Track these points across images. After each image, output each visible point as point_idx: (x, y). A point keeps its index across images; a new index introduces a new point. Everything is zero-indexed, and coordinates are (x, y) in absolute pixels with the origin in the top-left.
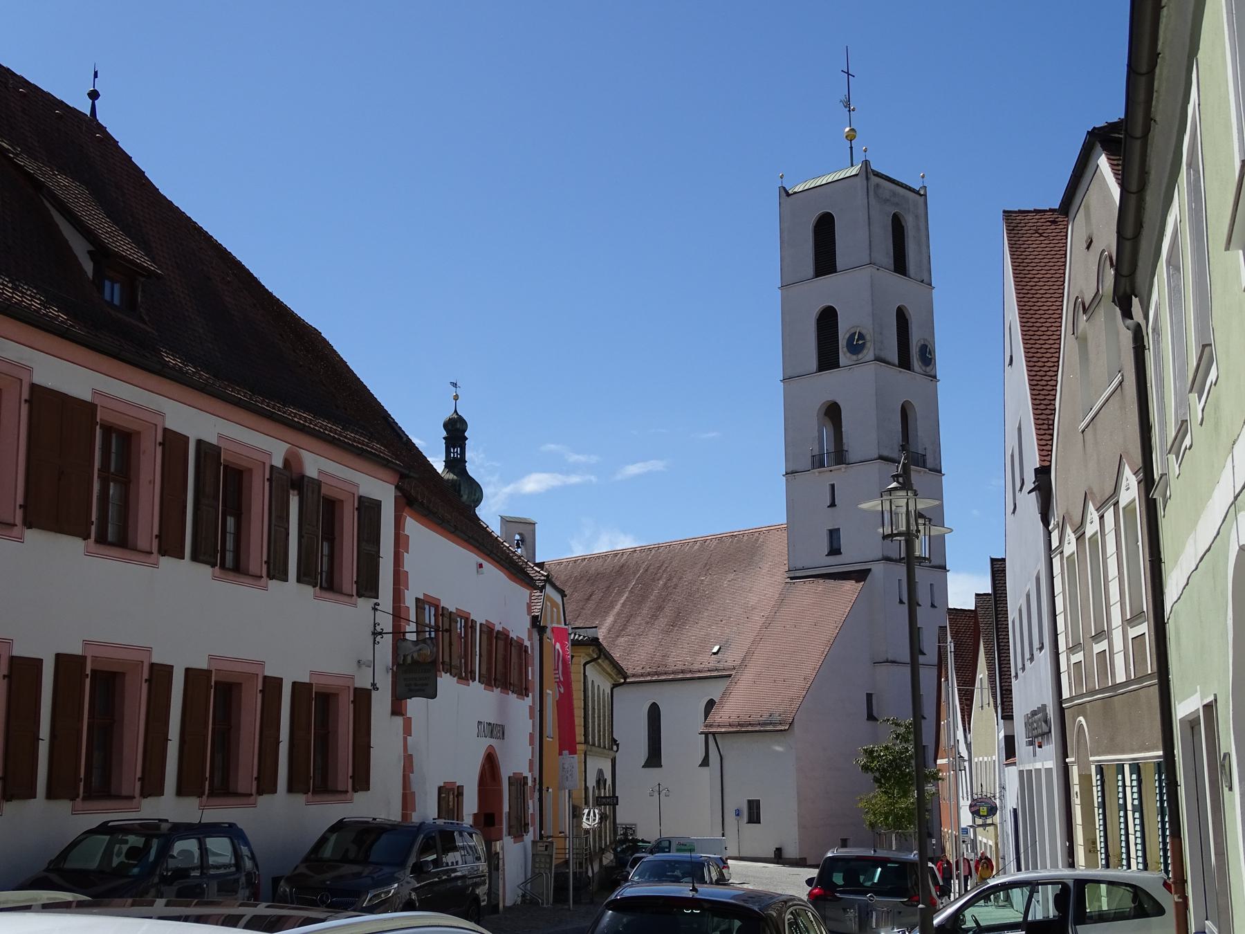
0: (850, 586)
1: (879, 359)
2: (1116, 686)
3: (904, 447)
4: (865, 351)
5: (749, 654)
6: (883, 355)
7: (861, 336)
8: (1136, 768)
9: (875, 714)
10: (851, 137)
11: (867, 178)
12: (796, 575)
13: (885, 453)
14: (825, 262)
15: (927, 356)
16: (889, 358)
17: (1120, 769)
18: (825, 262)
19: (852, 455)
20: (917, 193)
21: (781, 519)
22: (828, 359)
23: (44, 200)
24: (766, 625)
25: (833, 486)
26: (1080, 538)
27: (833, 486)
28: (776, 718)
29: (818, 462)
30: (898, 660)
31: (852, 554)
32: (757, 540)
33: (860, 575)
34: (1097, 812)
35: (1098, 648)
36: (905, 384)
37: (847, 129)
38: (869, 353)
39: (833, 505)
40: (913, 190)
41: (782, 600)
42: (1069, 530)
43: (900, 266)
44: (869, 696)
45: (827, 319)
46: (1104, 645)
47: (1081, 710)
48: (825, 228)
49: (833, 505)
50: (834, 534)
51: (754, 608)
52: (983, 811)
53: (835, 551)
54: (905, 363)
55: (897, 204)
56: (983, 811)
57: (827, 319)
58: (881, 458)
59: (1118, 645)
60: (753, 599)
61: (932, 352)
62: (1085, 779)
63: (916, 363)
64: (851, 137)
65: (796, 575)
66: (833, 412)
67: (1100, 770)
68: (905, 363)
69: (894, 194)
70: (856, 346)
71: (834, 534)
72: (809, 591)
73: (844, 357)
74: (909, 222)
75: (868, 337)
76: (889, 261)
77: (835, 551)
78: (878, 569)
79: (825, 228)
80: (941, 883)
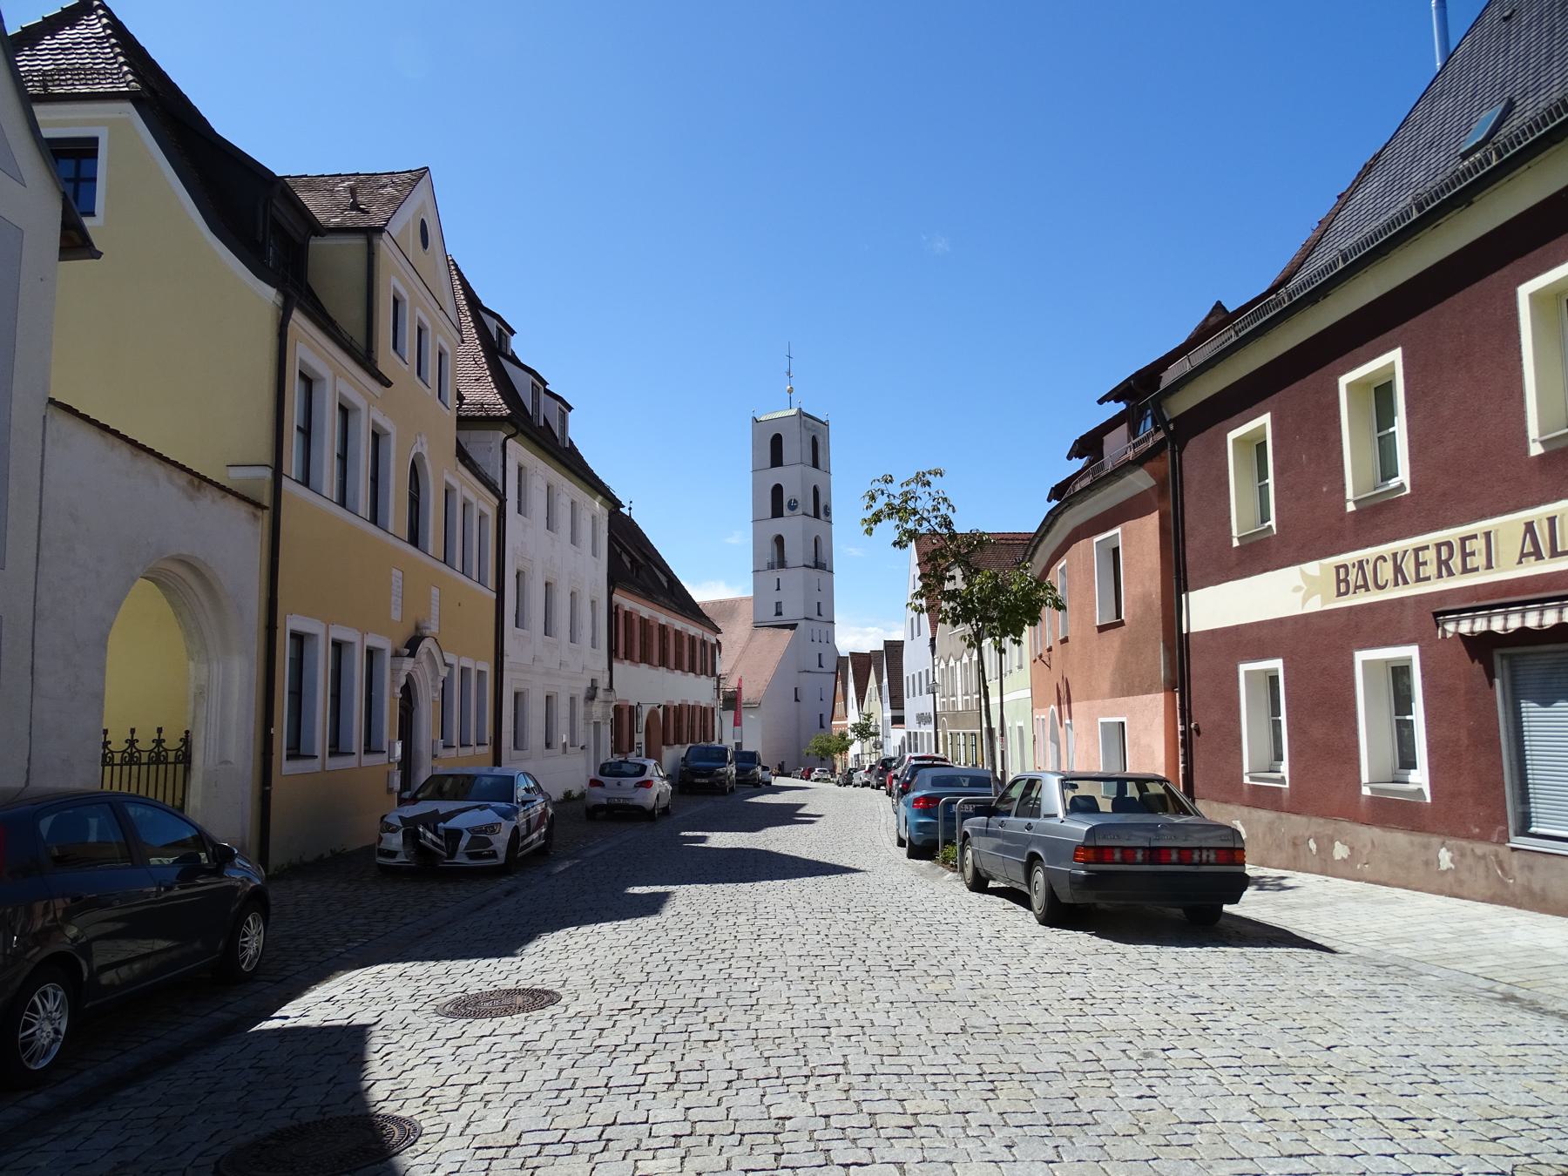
0: (787, 631)
1: (804, 514)
2: (958, 711)
3: (813, 559)
4: (797, 509)
5: (734, 666)
6: (806, 512)
7: (795, 501)
8: (964, 734)
9: (798, 698)
10: (790, 391)
11: (801, 417)
12: (758, 626)
13: (807, 563)
14: (777, 460)
15: (828, 512)
16: (809, 513)
17: (959, 734)
18: (777, 460)
19: (789, 564)
20: (824, 424)
21: (750, 594)
22: (777, 512)
23: (654, 569)
24: (743, 652)
25: (778, 579)
26: (947, 665)
27: (778, 579)
28: (751, 701)
29: (771, 567)
30: (810, 670)
31: (788, 616)
32: (735, 605)
33: (793, 627)
34: (949, 747)
35: (952, 699)
36: (816, 526)
37: (789, 387)
38: (799, 511)
39: (778, 589)
40: (821, 422)
41: (751, 639)
42: (942, 661)
43: (815, 465)
44: (796, 689)
45: (777, 491)
46: (954, 699)
47: (944, 716)
48: (777, 442)
49: (778, 589)
50: (778, 604)
51: (735, 642)
52: (878, 746)
53: (779, 613)
54: (817, 516)
55: (814, 431)
56: (878, 746)
57: (777, 491)
58: (805, 566)
59: (960, 699)
60: (734, 638)
61: (830, 509)
62: (945, 737)
63: (822, 515)
64: (790, 391)
65: (758, 626)
66: (779, 540)
67: (951, 734)
68: (817, 516)
69: (813, 425)
70: (792, 507)
71: (778, 604)
72: (765, 633)
73: (786, 511)
74: (820, 441)
75: (799, 502)
76: (811, 462)
77: (779, 613)
78: (802, 624)
79: (777, 442)
80: (616, 812)
